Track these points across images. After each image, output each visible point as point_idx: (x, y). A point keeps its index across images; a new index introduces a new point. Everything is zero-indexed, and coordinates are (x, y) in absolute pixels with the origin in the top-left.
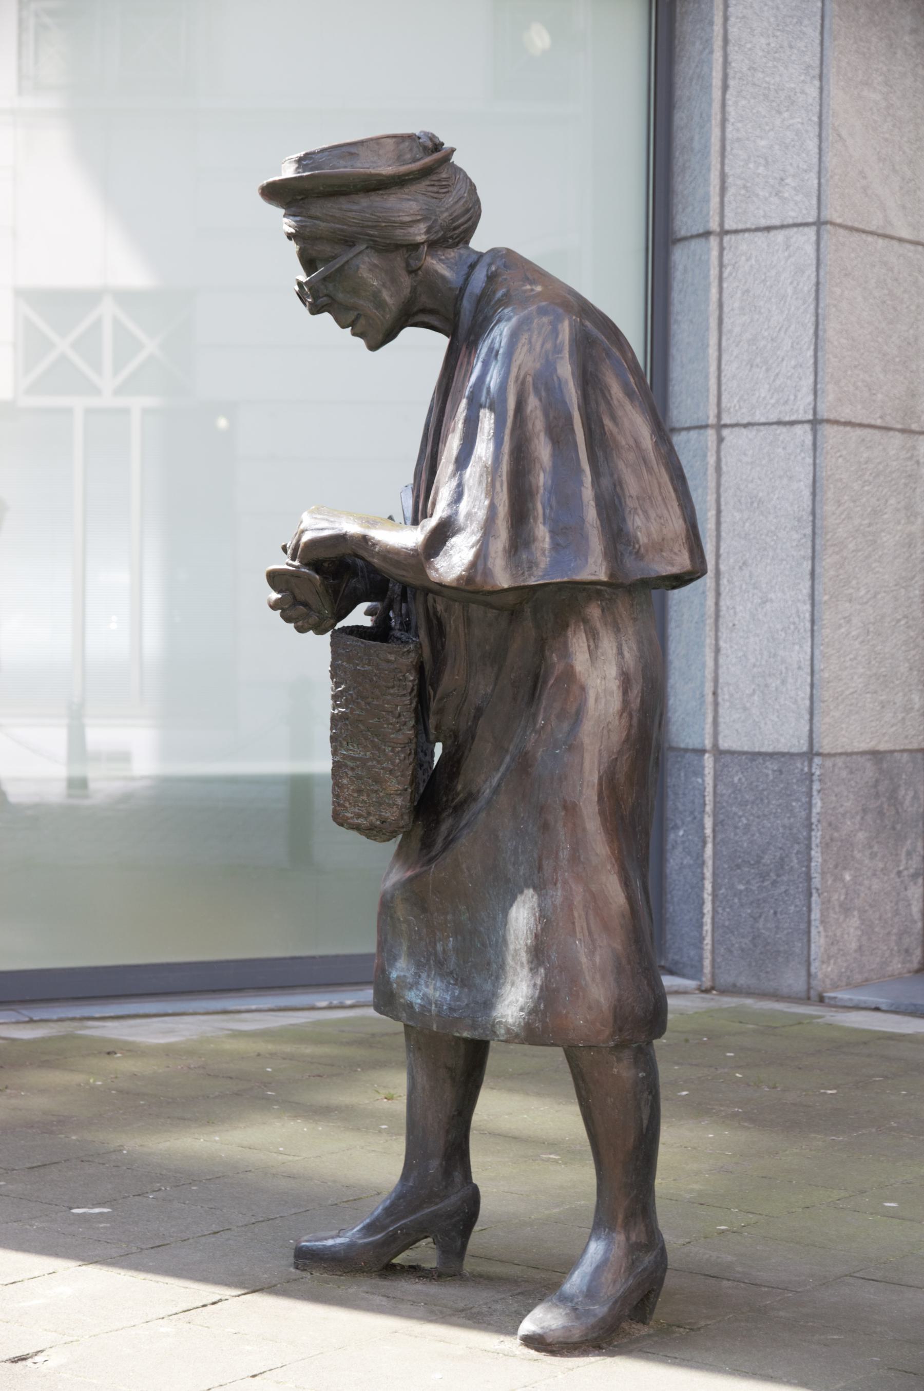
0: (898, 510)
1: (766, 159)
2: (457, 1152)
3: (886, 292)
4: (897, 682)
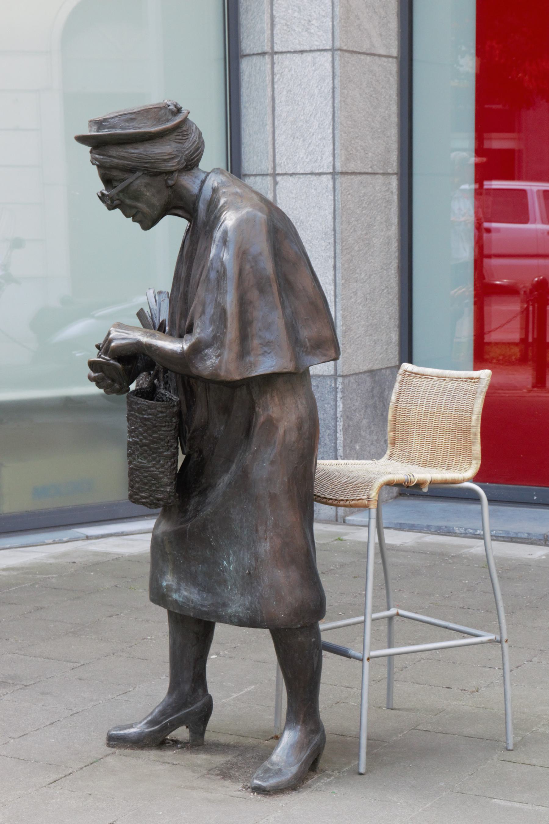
0: (381, 223)
1: (299, 7)
2: (200, 679)
3: (372, 89)
4: (383, 328)
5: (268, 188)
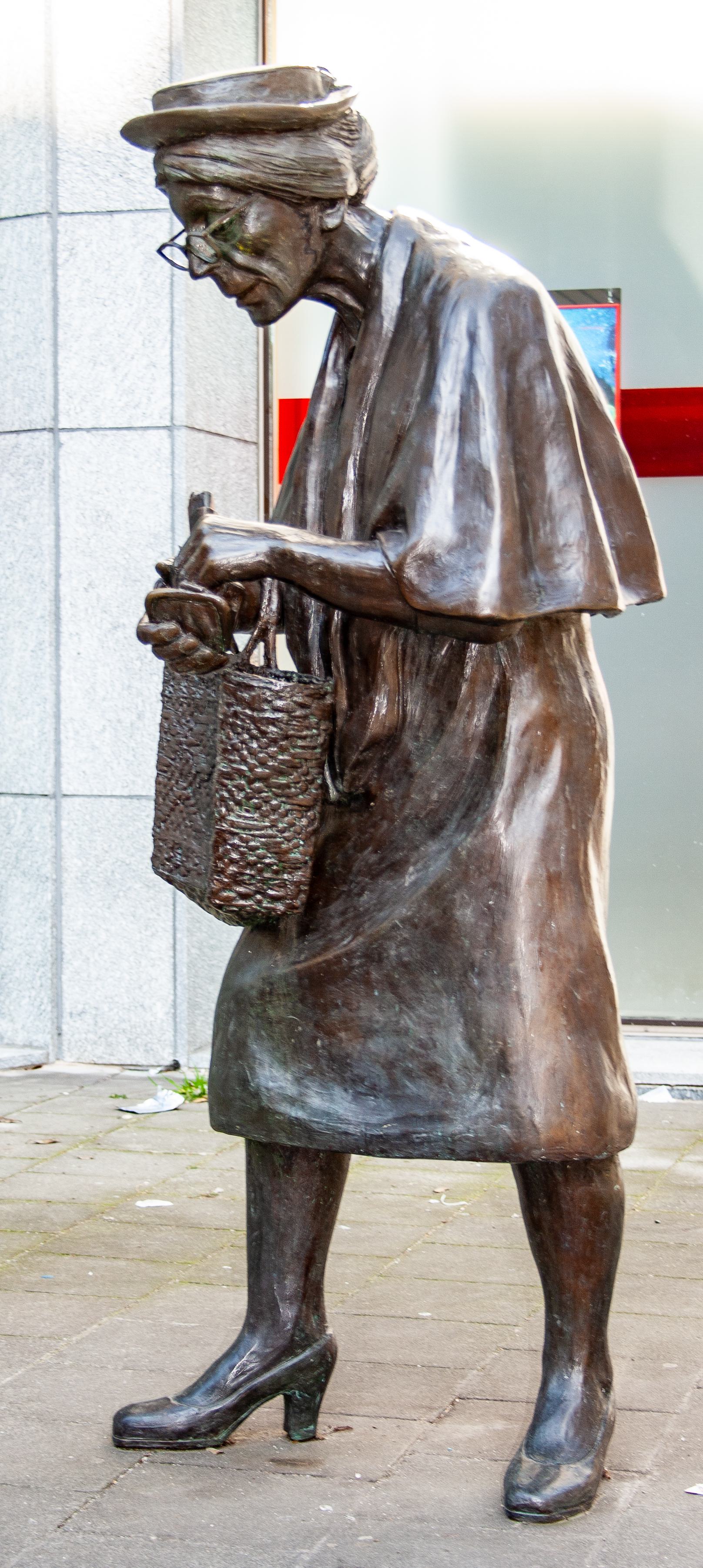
5: (44, 454)
